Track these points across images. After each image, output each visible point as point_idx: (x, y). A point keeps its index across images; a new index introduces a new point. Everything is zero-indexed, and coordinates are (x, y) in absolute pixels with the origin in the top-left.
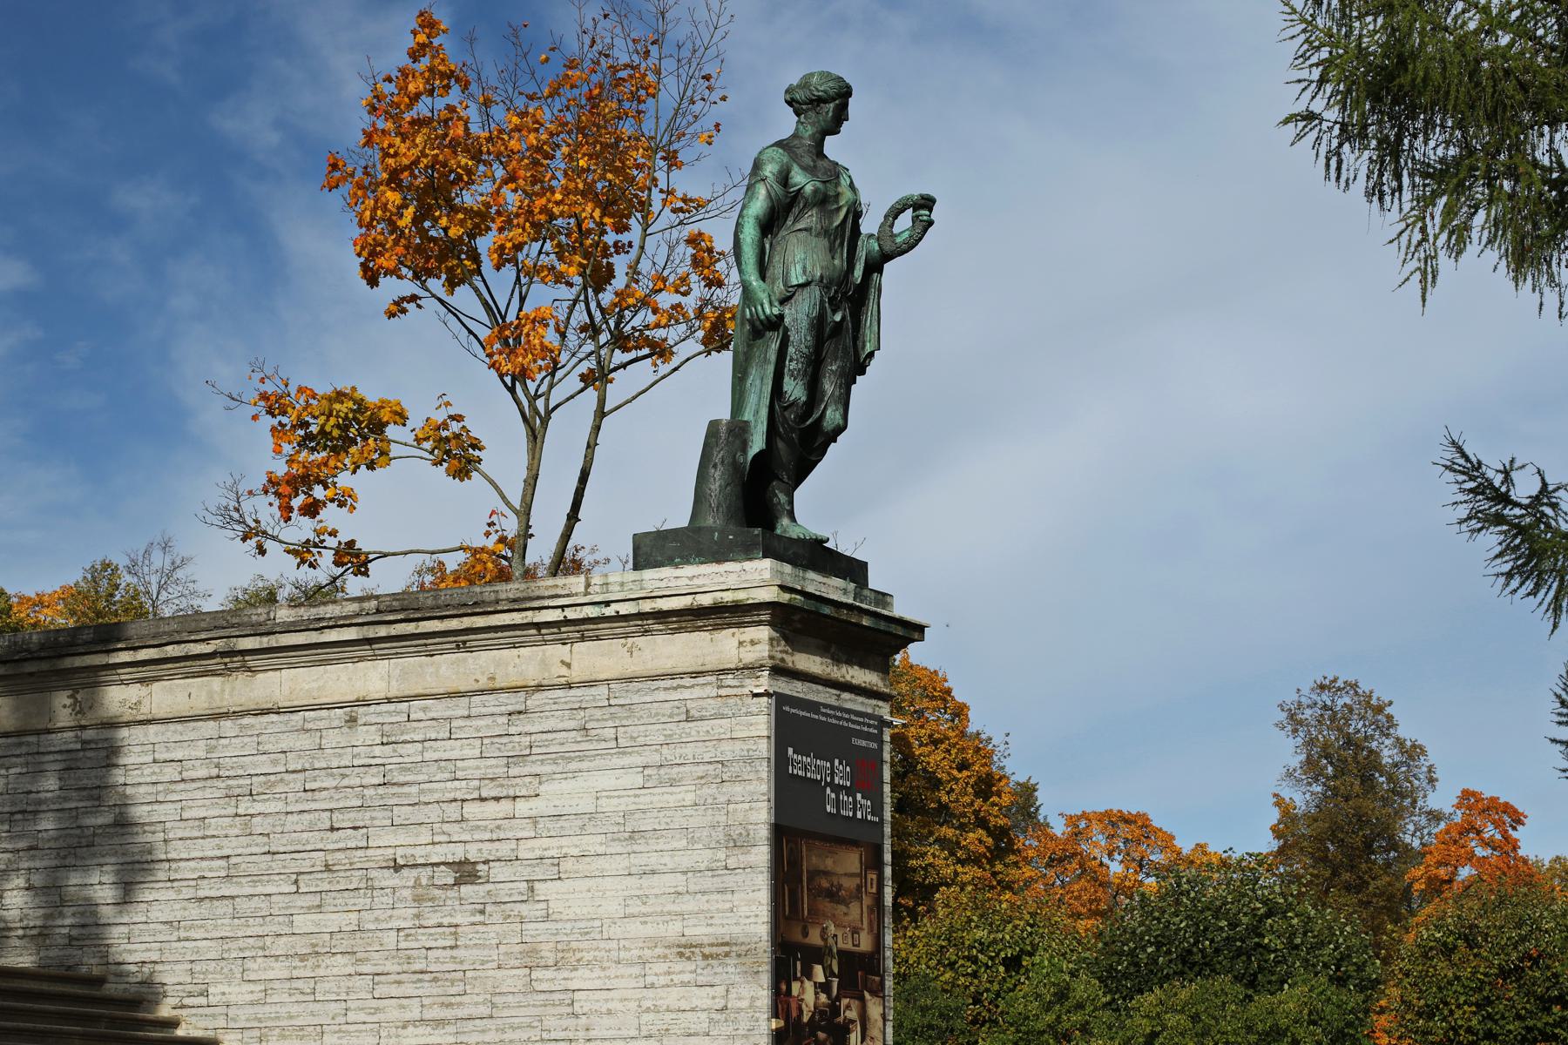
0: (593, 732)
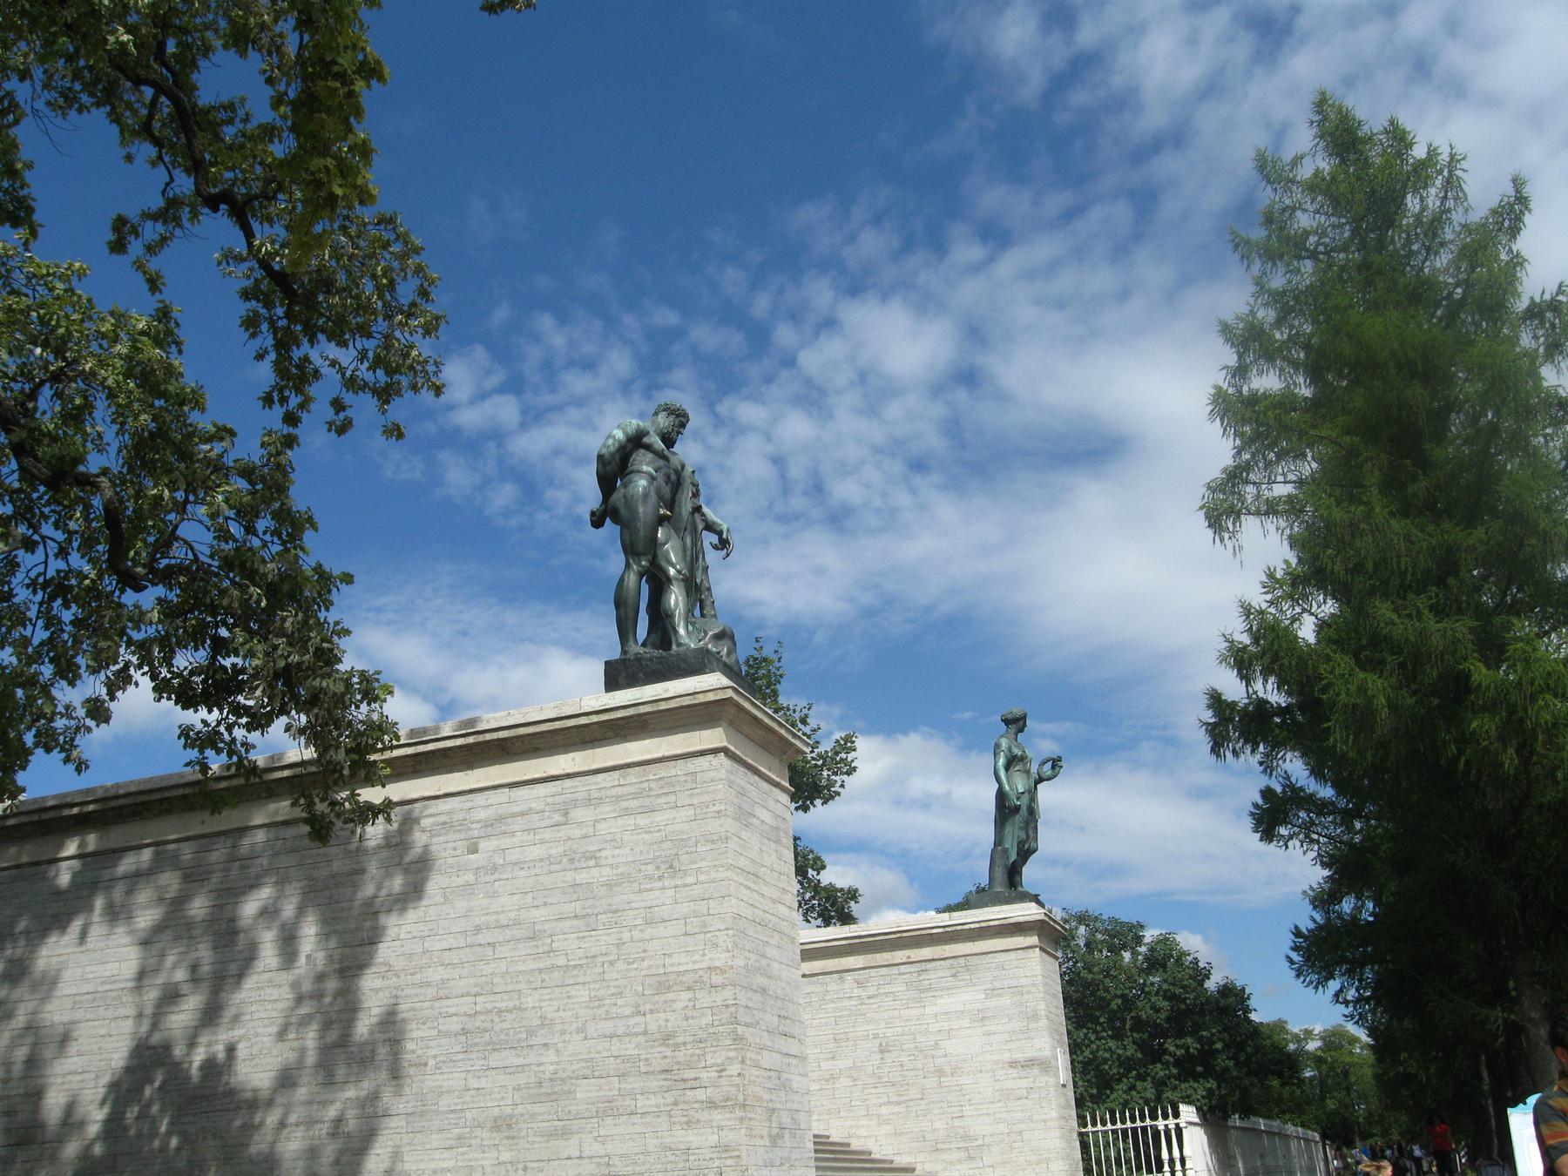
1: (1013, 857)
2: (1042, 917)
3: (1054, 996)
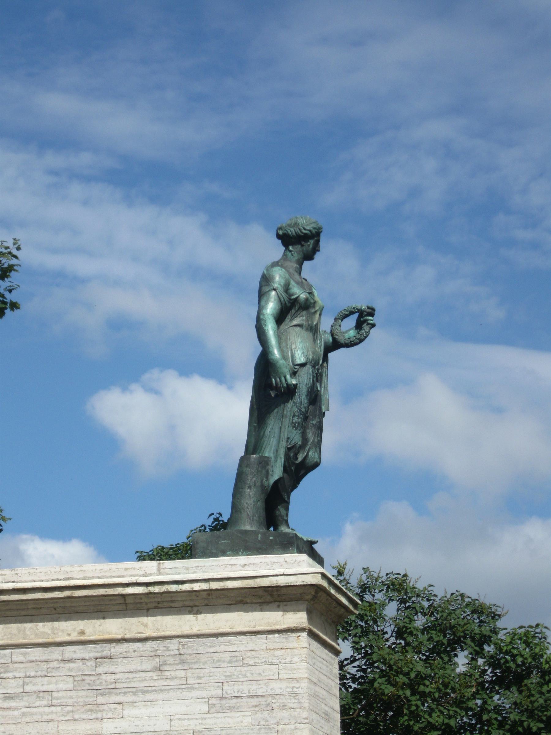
0: (167, 673)
1: (277, 473)
2: (317, 580)
3: (327, 717)
